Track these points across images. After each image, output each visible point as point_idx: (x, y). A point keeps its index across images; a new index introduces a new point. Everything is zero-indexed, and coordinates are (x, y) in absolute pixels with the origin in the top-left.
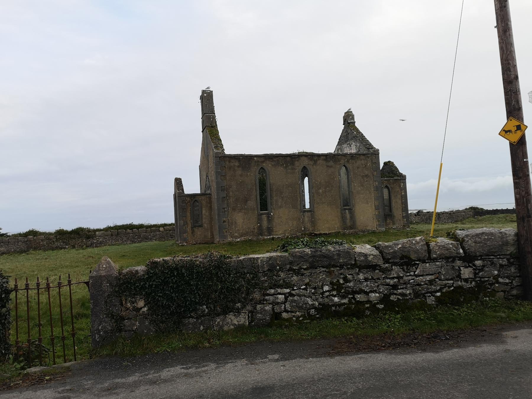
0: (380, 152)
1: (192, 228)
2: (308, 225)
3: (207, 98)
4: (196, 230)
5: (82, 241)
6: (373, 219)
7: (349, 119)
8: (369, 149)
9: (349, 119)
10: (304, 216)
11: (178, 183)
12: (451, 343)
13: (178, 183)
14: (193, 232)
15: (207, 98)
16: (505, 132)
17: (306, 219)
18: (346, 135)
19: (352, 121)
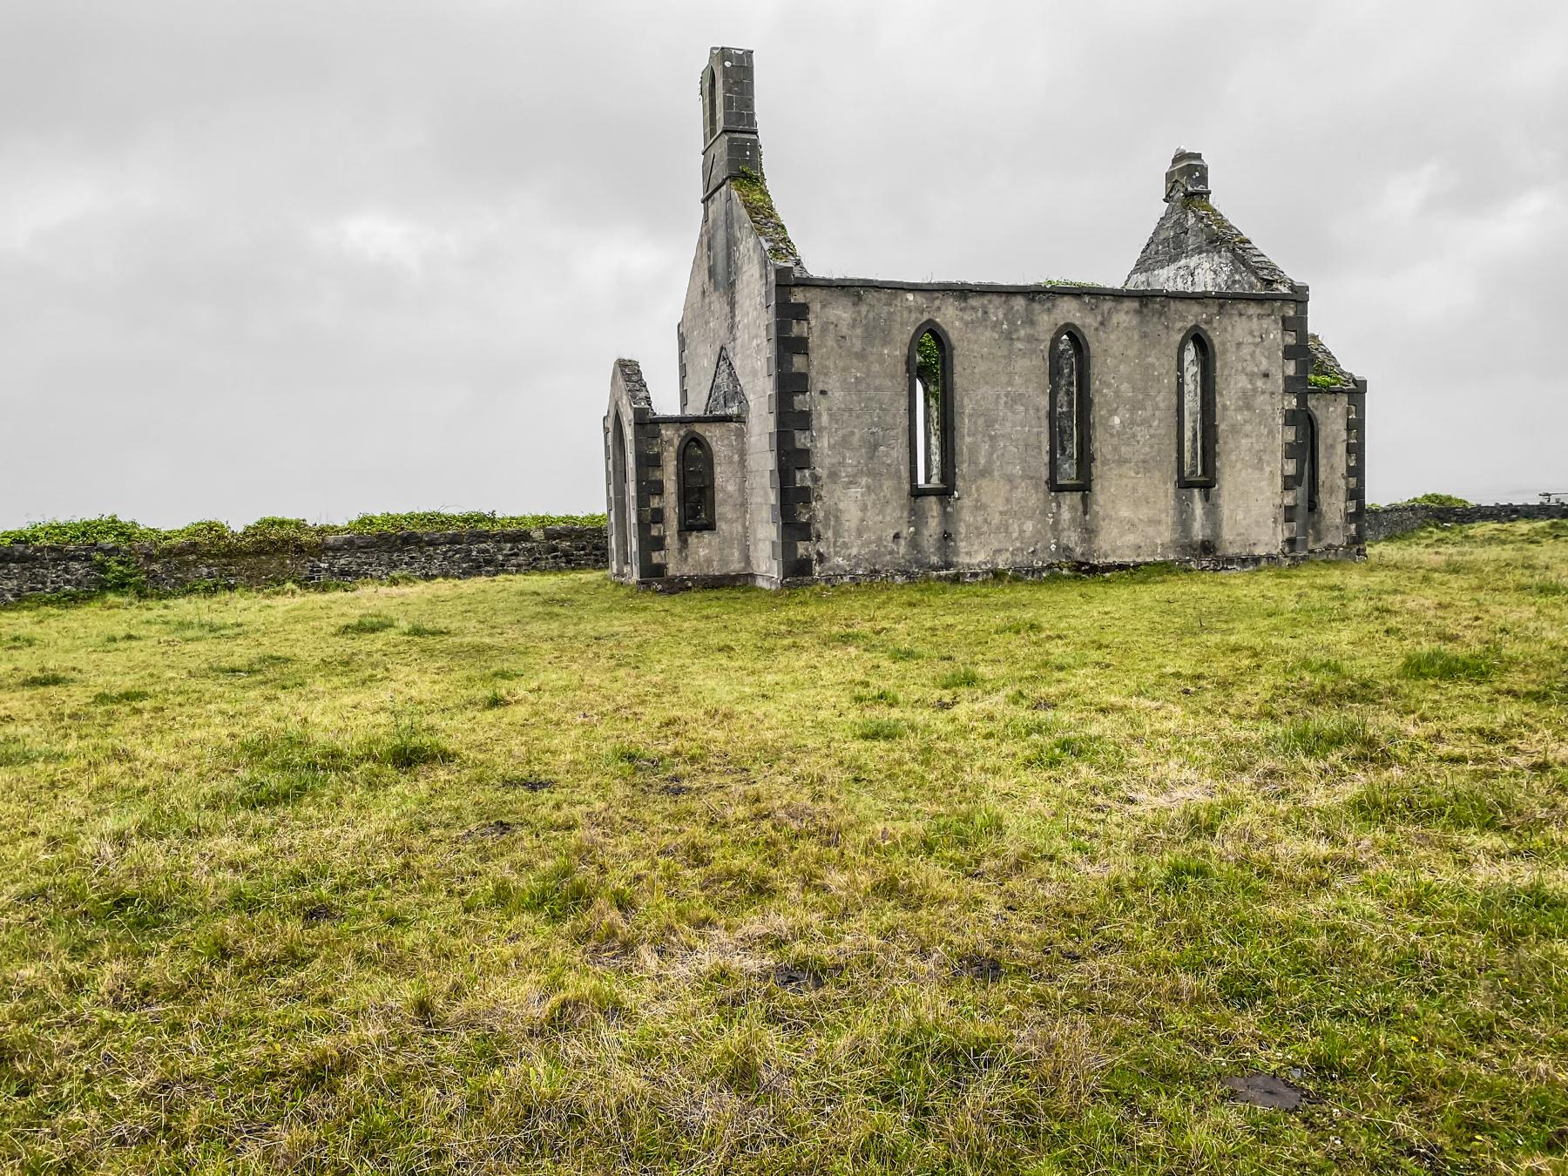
0: (1311, 293)
1: (680, 532)
2: (1072, 538)
3: (731, 80)
4: (693, 539)
5: (282, 564)
6: (1275, 522)
7: (1188, 180)
8: (1270, 283)
9: (1188, 180)
10: (1059, 506)
11: (628, 372)
12: (109, 541)
13: (628, 372)
14: (684, 543)
15: (731, 80)
16: (1299, 297)
17: (1066, 515)
18: (1177, 236)
19: (1200, 188)
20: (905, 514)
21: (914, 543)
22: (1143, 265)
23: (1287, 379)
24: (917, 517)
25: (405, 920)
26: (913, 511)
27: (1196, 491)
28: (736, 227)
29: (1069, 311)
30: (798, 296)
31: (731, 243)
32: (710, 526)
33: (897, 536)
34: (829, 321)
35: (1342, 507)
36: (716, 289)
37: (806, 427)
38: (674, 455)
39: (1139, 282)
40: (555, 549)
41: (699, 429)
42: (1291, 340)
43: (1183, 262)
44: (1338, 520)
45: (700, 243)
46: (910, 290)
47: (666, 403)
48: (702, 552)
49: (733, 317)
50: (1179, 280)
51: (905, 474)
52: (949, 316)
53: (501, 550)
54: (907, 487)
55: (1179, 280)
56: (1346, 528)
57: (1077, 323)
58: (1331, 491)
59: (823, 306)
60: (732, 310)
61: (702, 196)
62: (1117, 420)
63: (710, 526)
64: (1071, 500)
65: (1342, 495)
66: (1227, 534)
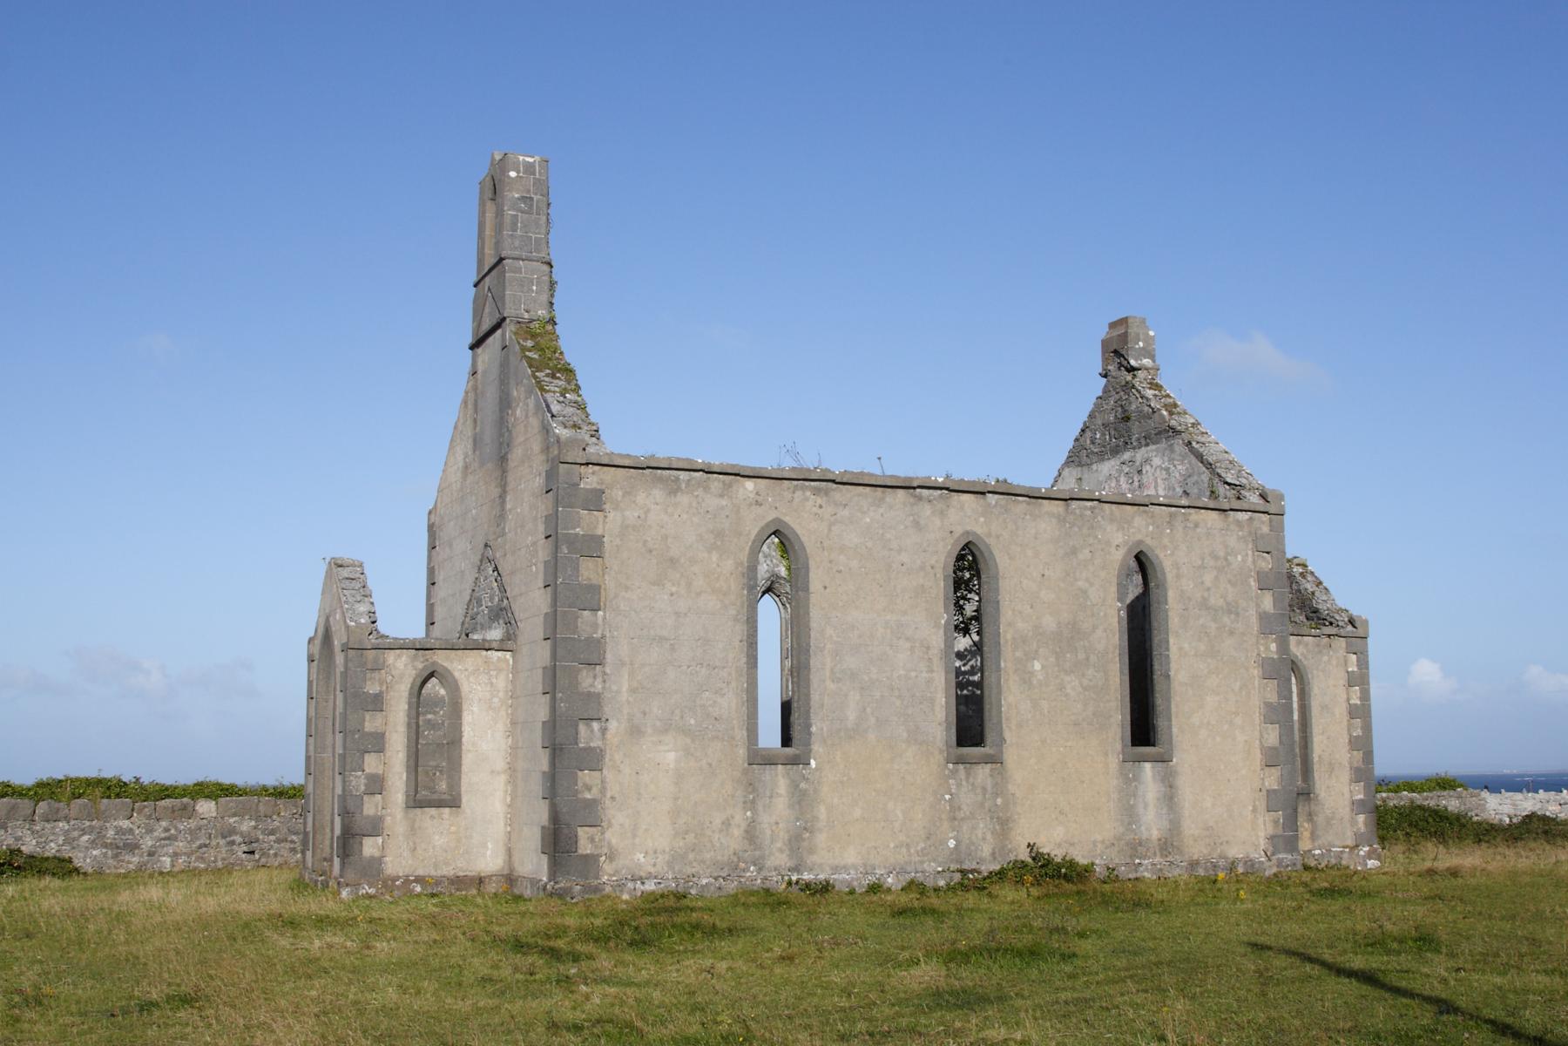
11: (345, 578)
13: (345, 578)
20: (739, 793)
21: (751, 835)
22: (1078, 457)
23: (1263, 617)
24: (752, 794)
25: (343, 798)
26: (751, 786)
27: (1148, 766)
28: (512, 382)
29: (967, 517)
30: (591, 479)
31: (505, 403)
32: (453, 802)
33: (727, 823)
34: (632, 518)
35: (1347, 795)
36: (482, 464)
37: (596, 662)
38: (406, 694)
39: (1069, 484)
40: (233, 831)
41: (441, 658)
42: (1266, 563)
43: (1127, 456)
44: (1344, 811)
45: (465, 402)
46: (417, 743)
47: (402, 617)
48: (439, 841)
49: (503, 503)
50: (1122, 479)
51: (741, 734)
52: (807, 516)
53: (150, 831)
54: (742, 752)
55: (1122, 479)
56: (1353, 822)
57: (979, 531)
58: (1331, 768)
59: (626, 494)
60: (502, 497)
61: (470, 340)
62: (1037, 666)
63: (453, 802)
64: (780, 779)
65: (1345, 776)
66: (1190, 828)
